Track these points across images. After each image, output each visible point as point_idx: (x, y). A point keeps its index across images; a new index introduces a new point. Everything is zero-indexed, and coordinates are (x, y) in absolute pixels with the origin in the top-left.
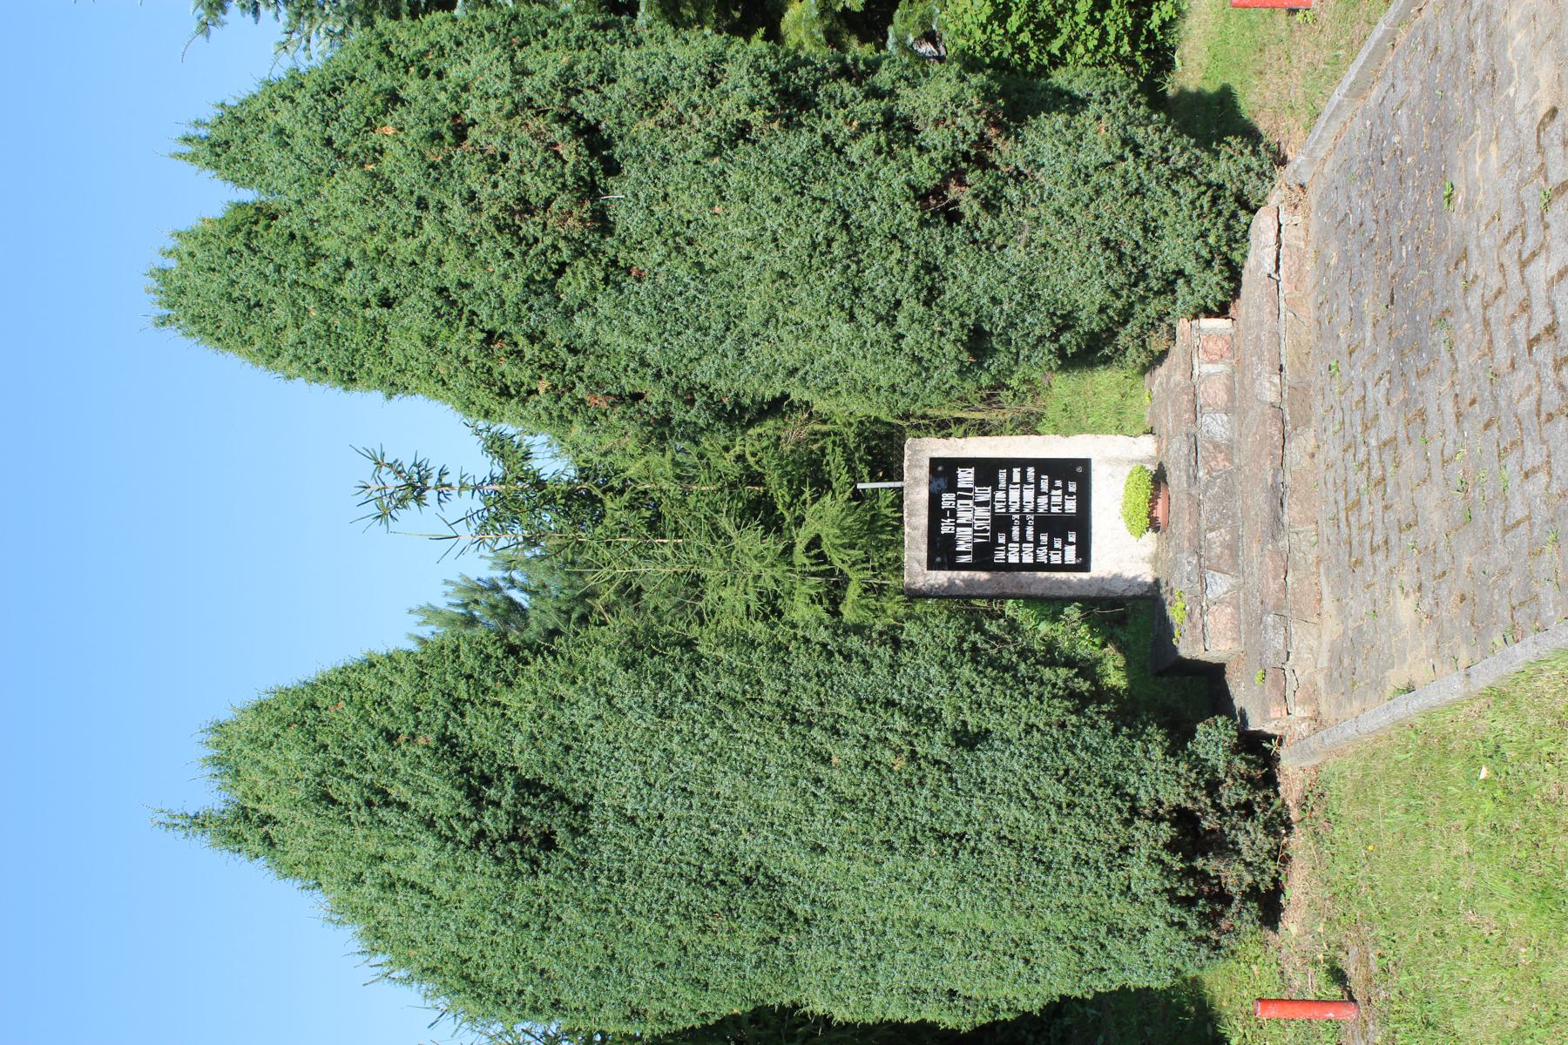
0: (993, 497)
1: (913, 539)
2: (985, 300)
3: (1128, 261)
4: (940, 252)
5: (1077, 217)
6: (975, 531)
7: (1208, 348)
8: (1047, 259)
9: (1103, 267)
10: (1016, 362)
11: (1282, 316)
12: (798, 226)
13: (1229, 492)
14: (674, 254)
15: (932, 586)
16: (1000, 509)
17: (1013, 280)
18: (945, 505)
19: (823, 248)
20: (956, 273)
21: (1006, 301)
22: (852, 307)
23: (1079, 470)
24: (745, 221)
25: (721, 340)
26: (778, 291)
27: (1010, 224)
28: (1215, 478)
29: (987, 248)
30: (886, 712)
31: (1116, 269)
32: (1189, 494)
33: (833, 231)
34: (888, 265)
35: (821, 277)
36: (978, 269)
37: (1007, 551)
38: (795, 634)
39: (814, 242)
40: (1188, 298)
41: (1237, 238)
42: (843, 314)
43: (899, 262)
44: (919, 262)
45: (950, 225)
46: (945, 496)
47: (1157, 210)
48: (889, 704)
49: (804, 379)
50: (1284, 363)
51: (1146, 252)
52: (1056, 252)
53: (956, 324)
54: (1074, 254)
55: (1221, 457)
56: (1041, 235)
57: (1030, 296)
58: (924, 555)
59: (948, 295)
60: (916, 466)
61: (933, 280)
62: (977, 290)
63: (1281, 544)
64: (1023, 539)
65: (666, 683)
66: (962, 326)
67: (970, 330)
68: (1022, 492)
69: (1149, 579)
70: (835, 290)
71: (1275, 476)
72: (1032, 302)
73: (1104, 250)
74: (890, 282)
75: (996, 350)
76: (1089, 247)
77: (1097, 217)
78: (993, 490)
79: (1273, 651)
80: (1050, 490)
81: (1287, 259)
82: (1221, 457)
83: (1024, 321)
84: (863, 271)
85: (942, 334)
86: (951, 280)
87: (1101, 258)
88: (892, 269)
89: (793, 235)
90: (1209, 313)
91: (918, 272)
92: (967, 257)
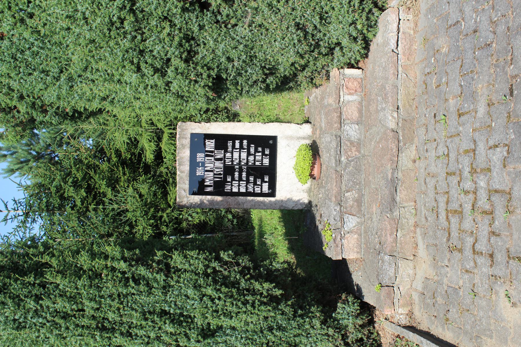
0: (225, 156)
1: (181, 178)
2: (223, 60)
3: (310, 37)
4: (196, 29)
5: (281, 9)
6: (215, 174)
7: (349, 86)
8: (262, 34)
9: (296, 41)
10: (241, 94)
11: (399, 76)
12: (99, 9)
13: (358, 170)
14: (18, 24)
15: (192, 203)
16: (228, 162)
17: (241, 47)
18: (199, 160)
19: (118, 25)
20: (206, 42)
21: (236, 59)
22: (139, 62)
23: (271, 142)
24: (63, 5)
25: (58, 79)
26: (90, 51)
27: (240, 11)
28: (350, 161)
29: (225, 26)
30: (161, 320)
31: (303, 42)
32: (336, 171)
33: (123, 14)
34: (161, 36)
35: (117, 44)
36: (219, 39)
37: (232, 186)
38: (106, 265)
39: (111, 21)
40: (341, 58)
41: (372, 25)
42: (133, 67)
43: (169, 35)
44: (181, 35)
45: (202, 11)
46: (199, 155)
47: (328, 6)
48: (163, 313)
49: (112, 102)
50: (399, 105)
51: (320, 32)
52: (267, 30)
53: (205, 76)
54: (278, 32)
55: (354, 149)
56: (259, 19)
57: (251, 57)
58: (187, 186)
59: (200, 56)
60: (183, 138)
61: (191, 46)
62: (219, 53)
63: (395, 214)
64: (240, 179)
65: (22, 304)
66: (209, 76)
67: (213, 79)
68: (240, 154)
69: (306, 201)
70: (127, 51)
71: (393, 173)
72: (252, 60)
73: (297, 30)
74: (163, 47)
75: (228, 89)
76: (288, 28)
77: (293, 9)
78: (225, 152)
79: (388, 277)
80: (255, 153)
81: (403, 41)
82: (354, 149)
83: (246, 72)
84: (145, 40)
85: (196, 82)
86: (202, 46)
87: (295, 35)
88: (164, 39)
89: (97, 15)
90: (351, 66)
91: (181, 41)
92: (213, 32)
